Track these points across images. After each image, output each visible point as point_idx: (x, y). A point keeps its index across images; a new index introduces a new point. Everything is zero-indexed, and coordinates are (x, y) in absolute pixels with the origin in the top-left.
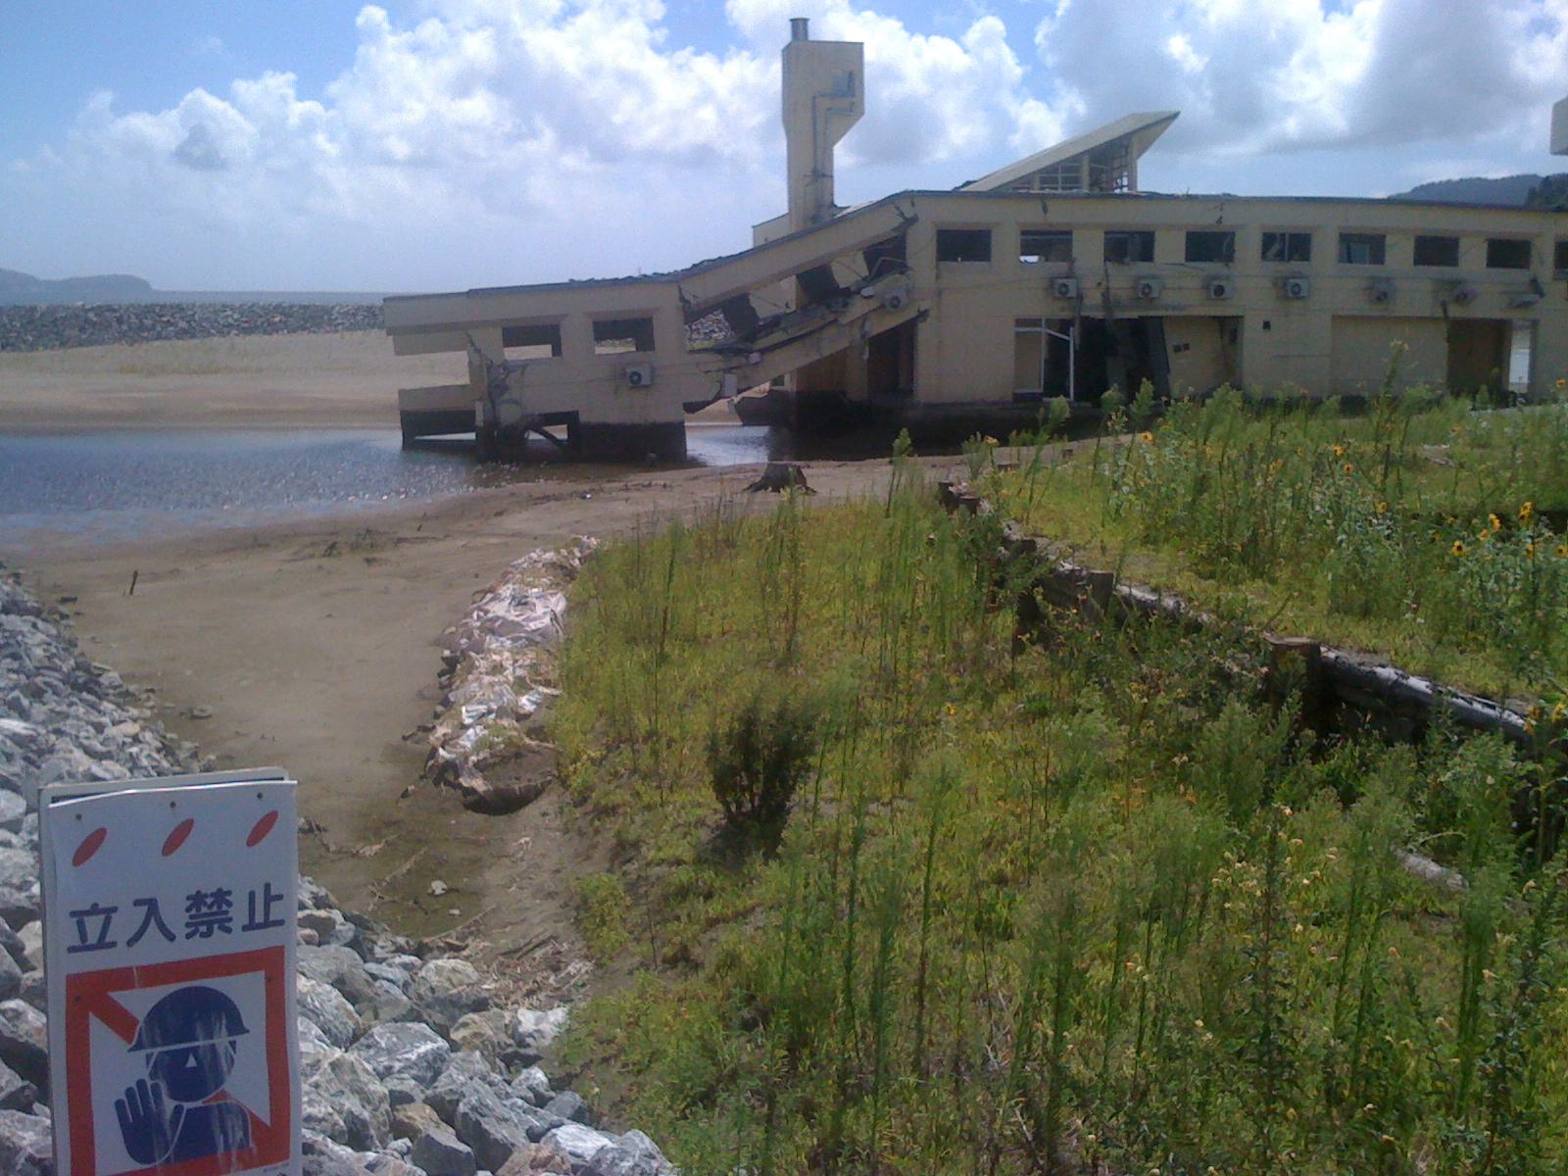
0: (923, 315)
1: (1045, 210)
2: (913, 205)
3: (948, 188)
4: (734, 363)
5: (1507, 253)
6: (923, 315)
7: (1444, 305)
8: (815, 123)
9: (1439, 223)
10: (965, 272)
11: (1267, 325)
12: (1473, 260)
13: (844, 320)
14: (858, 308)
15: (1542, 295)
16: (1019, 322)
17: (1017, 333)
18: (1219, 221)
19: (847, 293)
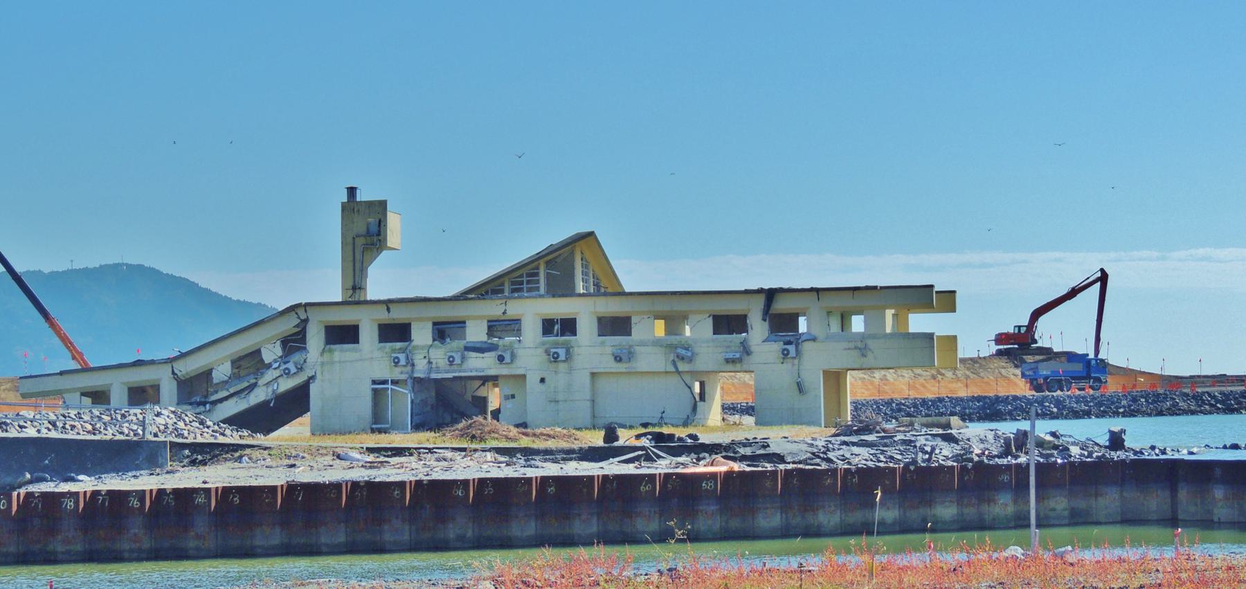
0: (312, 378)
6: (312, 378)
7: (674, 363)
10: (342, 352)
11: (542, 380)
12: (422, 335)
13: (261, 382)
14: (270, 375)
16: (374, 382)
18: (504, 313)
19: (269, 366)
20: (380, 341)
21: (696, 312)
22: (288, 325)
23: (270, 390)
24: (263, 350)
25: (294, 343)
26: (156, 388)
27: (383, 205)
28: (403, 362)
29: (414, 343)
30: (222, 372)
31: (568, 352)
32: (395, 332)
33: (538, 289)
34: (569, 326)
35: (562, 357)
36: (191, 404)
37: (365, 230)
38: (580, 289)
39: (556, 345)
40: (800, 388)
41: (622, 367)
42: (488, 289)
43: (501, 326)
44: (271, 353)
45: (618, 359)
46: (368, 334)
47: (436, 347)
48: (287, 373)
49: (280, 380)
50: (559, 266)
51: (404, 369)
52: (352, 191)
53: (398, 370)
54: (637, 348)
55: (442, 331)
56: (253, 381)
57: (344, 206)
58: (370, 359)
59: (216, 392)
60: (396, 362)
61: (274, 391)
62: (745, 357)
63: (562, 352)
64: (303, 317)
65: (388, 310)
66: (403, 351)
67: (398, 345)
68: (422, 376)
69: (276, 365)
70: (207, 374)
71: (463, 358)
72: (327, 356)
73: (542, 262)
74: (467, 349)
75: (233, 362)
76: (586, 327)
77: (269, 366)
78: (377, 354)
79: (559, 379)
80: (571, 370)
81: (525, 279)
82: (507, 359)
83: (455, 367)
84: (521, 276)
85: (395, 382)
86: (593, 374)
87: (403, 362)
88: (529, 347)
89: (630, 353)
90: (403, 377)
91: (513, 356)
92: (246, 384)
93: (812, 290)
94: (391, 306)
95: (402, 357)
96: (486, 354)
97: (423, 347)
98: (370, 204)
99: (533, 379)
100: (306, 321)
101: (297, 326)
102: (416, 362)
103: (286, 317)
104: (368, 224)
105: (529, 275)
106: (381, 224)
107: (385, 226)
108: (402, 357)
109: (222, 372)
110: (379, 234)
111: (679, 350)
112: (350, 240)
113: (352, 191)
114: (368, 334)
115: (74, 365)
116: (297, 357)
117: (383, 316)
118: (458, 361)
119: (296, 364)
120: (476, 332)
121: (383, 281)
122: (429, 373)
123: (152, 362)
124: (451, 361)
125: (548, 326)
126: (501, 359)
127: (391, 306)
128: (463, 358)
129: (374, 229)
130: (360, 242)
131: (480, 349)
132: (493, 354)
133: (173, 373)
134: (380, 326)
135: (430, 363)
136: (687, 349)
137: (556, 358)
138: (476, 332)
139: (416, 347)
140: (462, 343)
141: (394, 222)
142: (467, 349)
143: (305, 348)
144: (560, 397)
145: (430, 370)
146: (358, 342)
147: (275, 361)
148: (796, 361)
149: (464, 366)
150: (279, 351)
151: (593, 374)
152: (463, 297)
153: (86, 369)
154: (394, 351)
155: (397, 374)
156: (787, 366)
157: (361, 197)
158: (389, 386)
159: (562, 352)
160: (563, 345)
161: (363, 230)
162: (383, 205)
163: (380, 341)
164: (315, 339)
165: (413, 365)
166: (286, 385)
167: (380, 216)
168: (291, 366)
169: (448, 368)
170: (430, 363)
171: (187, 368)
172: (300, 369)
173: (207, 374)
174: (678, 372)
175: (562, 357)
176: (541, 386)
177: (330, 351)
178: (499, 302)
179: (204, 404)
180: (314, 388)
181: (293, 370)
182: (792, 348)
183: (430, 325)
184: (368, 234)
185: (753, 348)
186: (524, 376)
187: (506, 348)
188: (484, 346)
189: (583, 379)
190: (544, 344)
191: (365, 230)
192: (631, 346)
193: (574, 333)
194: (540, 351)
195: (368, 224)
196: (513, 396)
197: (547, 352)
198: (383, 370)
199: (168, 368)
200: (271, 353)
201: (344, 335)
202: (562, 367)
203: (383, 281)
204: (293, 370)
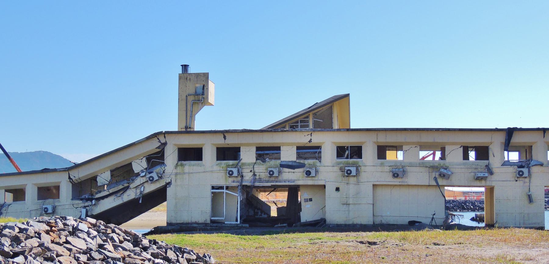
0: (169, 184)
1: (225, 137)
2: (165, 137)
3: (259, 129)
4: (86, 204)
5: (265, 152)
6: (169, 184)
7: (436, 179)
8: (187, 106)
9: (231, 141)
10: (190, 166)
11: (338, 189)
12: (248, 156)
13: (132, 186)
14: (139, 181)
15: (491, 173)
16: (213, 188)
17: (212, 193)
18: (310, 141)
19: (138, 175)
20: (217, 160)
21: (408, 144)
22: (153, 147)
23: (138, 191)
24: (133, 163)
25: (156, 159)
26: (58, 188)
27: (206, 76)
28: (235, 174)
29: (242, 161)
30: (104, 178)
31: (357, 170)
32: (228, 153)
33: (308, 126)
34: (357, 152)
35: (354, 173)
36: (82, 200)
37: (194, 92)
38: (336, 126)
39: (348, 165)
40: (530, 199)
41: (397, 181)
42: (294, 123)
43: (310, 152)
44: (139, 166)
45: (395, 175)
46: (209, 154)
47: (260, 164)
48: (151, 180)
49: (146, 185)
50: (326, 114)
51: (235, 179)
52: (185, 67)
53: (231, 180)
54: (408, 169)
55: (265, 152)
56: (126, 185)
57: (180, 78)
58: (210, 171)
59: (100, 192)
60: (231, 174)
61: (141, 192)
62: (490, 177)
63: (353, 170)
64: (163, 141)
65: (225, 137)
66: (236, 166)
67: (231, 162)
68: (248, 184)
69: (143, 174)
70: (94, 179)
71: (280, 172)
72: (179, 169)
73: (311, 114)
74: (282, 166)
75: (112, 171)
76: (329, 154)
77: (138, 175)
78: (216, 168)
79: (350, 188)
80: (358, 183)
81: (299, 124)
82: (313, 174)
83: (273, 179)
84: (297, 122)
85: (227, 188)
86: (374, 186)
87: (235, 174)
88: (328, 167)
89: (404, 171)
90: (235, 184)
91: (317, 172)
92: (121, 187)
93: (538, 129)
94: (226, 134)
95: (235, 171)
96: (296, 170)
97: (249, 164)
98: (197, 75)
99: (330, 189)
100: (165, 144)
101: (158, 148)
102: (244, 174)
103: (150, 141)
104: (196, 88)
105: (301, 121)
106: (205, 88)
107: (208, 89)
108: (235, 171)
109: (104, 178)
110: (203, 94)
111: (442, 170)
112: (184, 97)
113: (185, 67)
114: (209, 154)
115: (16, 171)
116: (158, 169)
117: (220, 141)
118: (276, 174)
119: (157, 174)
120: (288, 155)
121: (203, 121)
122: (254, 182)
123: (55, 170)
124: (271, 174)
125: (341, 151)
126: (308, 173)
127: (226, 134)
128: (280, 172)
129: (200, 91)
130: (191, 98)
131: (291, 166)
132: (301, 170)
133: (70, 178)
134: (218, 149)
135: (254, 175)
136: (446, 169)
137: (349, 173)
138: (288, 155)
139: (244, 164)
140: (278, 162)
141: (211, 87)
142: (282, 166)
143: (163, 163)
144: (351, 201)
145: (255, 180)
146: (202, 160)
147: (142, 171)
148: (527, 180)
149: (280, 178)
150: (144, 164)
151: (374, 186)
152: (274, 129)
153: (20, 173)
154: (228, 166)
155: (230, 182)
156: (520, 183)
157: (191, 70)
158: (225, 191)
159: (353, 170)
160: (353, 165)
161: (192, 91)
162: (206, 76)
163: (217, 160)
164: (171, 156)
165: (242, 176)
166: (150, 188)
167: (204, 83)
168: (154, 175)
169: (267, 179)
170: (254, 175)
171: (78, 175)
172: (160, 178)
173: (94, 179)
174: (438, 186)
175: (354, 173)
176: (338, 194)
177: (182, 165)
178: (306, 134)
179: (91, 200)
180: (169, 191)
181: (156, 178)
182: (525, 170)
183: (295, 148)
184: (196, 94)
185: (494, 170)
186: (325, 186)
187: (311, 166)
188: (294, 164)
189: (367, 189)
190: (339, 164)
191: (194, 92)
192: (403, 167)
193: (319, 158)
194: (337, 169)
195: (196, 88)
196: (311, 200)
197: (341, 169)
198: (221, 180)
199: (65, 175)
200: (139, 166)
201: (191, 154)
202: (352, 180)
203: (203, 121)
204: (156, 178)
